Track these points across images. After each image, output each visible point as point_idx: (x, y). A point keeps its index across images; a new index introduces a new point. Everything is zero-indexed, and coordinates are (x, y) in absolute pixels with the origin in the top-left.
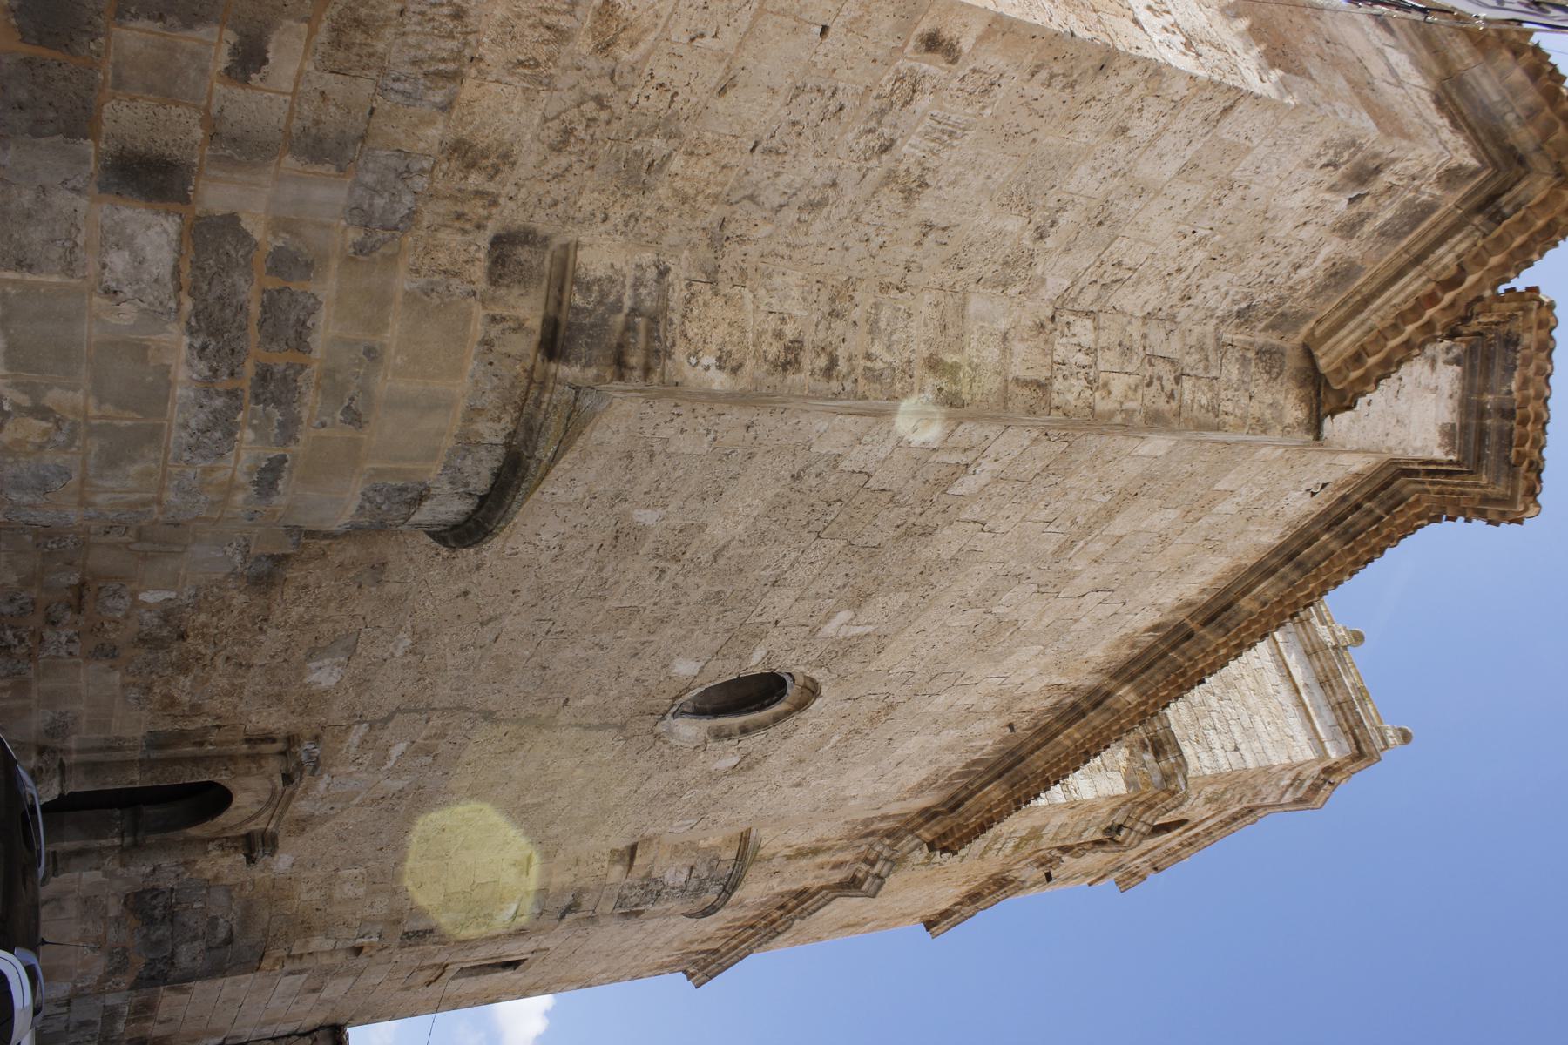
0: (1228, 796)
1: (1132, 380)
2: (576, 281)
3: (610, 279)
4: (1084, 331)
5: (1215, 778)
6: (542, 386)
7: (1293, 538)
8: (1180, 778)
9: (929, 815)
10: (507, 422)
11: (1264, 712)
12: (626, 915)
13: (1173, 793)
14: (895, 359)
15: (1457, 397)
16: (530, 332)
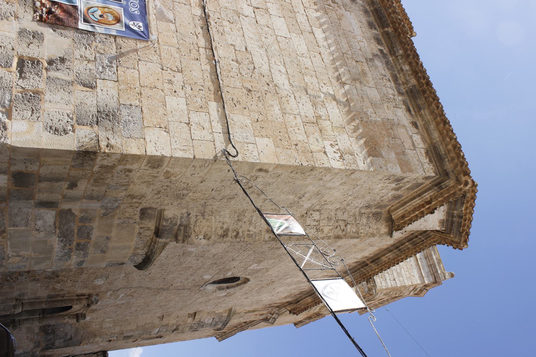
0: (391, 293)
1: (331, 228)
2: (164, 219)
3: (174, 218)
4: (316, 216)
5: (386, 289)
6: (155, 243)
7: (397, 243)
8: (374, 290)
9: (290, 303)
10: (146, 250)
11: (405, 267)
12: (193, 331)
13: (371, 295)
14: (257, 231)
15: (446, 211)
16: (152, 230)
